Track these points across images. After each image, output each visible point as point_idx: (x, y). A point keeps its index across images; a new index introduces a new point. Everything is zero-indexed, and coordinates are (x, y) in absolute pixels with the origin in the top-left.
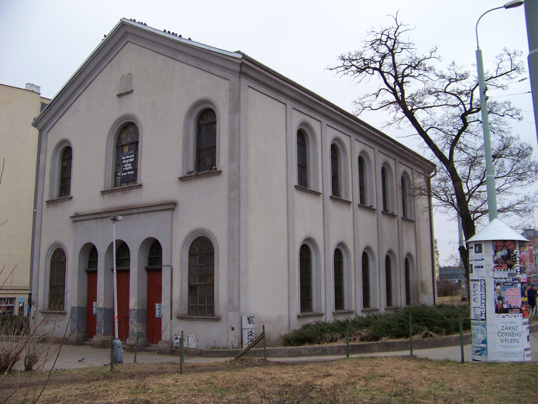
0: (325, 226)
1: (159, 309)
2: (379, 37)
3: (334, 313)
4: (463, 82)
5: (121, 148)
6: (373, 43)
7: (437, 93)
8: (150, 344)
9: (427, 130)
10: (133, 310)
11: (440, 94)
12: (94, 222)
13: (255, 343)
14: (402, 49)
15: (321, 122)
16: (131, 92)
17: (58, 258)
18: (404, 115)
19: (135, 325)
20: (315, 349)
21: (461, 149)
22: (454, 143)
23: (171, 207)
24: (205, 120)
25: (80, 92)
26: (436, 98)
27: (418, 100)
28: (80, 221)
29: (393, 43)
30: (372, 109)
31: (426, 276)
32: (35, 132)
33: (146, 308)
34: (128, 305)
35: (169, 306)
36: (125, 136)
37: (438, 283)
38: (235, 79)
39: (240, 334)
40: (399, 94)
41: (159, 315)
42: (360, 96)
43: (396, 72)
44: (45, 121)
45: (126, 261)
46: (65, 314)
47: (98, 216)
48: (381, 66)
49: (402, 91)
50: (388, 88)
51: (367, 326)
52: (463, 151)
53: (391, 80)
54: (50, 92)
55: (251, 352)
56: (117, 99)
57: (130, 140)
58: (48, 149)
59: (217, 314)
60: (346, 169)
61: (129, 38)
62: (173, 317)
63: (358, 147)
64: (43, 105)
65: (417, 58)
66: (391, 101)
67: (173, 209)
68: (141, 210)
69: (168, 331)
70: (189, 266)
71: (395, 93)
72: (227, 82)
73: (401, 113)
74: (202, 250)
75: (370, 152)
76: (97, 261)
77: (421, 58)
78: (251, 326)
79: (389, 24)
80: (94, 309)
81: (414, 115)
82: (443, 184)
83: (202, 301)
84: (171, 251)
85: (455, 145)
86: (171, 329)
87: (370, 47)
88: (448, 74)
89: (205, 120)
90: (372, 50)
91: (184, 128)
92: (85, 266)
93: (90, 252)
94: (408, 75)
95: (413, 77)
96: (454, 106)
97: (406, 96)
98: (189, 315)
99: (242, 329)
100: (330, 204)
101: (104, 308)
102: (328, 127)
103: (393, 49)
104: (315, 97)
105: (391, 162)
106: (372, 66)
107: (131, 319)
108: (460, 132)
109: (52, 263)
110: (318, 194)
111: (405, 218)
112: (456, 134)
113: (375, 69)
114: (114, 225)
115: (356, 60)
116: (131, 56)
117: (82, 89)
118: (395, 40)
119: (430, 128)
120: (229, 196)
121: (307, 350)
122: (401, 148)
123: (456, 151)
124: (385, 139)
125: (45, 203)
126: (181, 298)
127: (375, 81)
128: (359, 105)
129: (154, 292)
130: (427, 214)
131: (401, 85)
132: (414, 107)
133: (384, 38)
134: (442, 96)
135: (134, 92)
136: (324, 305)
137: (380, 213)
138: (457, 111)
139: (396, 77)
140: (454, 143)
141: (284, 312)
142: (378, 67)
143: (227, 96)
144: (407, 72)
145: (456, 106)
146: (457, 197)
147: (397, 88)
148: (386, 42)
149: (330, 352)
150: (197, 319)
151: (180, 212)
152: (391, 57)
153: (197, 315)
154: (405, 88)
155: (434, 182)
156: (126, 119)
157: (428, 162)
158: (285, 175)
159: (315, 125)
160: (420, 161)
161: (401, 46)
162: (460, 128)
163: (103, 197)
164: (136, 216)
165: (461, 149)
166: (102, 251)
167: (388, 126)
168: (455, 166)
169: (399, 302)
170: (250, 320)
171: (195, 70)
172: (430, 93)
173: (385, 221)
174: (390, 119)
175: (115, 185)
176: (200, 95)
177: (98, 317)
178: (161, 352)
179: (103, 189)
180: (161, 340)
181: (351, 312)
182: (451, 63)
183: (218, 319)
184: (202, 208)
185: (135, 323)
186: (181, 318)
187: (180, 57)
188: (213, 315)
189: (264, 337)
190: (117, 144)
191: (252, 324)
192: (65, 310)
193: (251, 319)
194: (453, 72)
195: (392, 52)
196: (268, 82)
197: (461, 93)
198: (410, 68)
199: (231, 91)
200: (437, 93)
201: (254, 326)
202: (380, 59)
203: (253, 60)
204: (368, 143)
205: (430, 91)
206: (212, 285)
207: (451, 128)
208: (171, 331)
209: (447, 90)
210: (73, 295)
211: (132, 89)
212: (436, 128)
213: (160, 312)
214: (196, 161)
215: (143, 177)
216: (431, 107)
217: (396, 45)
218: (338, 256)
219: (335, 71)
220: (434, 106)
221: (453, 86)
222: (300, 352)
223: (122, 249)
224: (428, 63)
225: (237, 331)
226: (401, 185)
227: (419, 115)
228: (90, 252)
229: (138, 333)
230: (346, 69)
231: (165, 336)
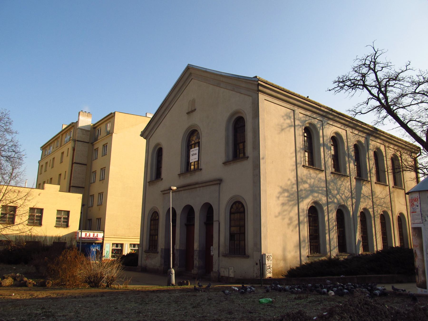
9: (407, 123)
14: (382, 68)
23: (218, 182)
25: (166, 113)
42: (353, 103)
46: (158, 253)
49: (386, 98)
53: (375, 91)
62: (220, 256)
67: (220, 184)
68: (201, 185)
71: (378, 99)
88: (416, 79)
91: (327, 107)
116: (194, 88)
125: (148, 183)
147: (381, 96)
154: (388, 94)
164: (198, 189)
166: (179, 212)
180: (212, 271)
183: (248, 257)
185: (197, 259)
186: (225, 256)
194: (421, 78)
208: (219, 265)
212: (415, 121)
227: (400, 113)
231: (215, 268)
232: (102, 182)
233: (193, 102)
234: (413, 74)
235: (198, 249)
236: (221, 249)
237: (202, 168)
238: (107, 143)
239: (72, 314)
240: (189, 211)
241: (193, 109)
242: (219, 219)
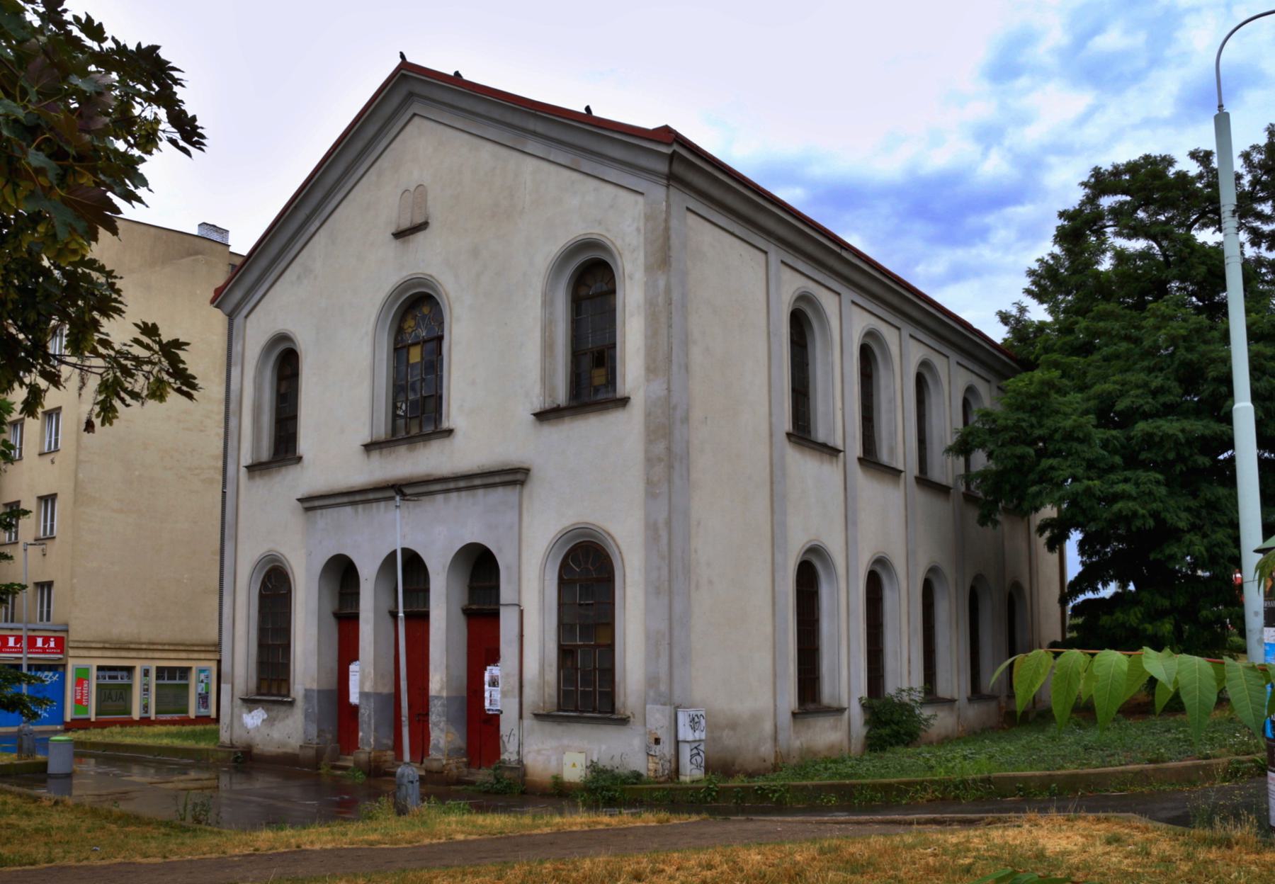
0: (849, 520)
5: (405, 351)
10: (437, 697)
12: (349, 509)
15: (839, 294)
17: (275, 585)
19: (442, 730)
23: (519, 477)
24: (589, 279)
25: (313, 229)
28: (321, 507)
33: (465, 694)
38: (658, 192)
39: (673, 752)
44: (238, 295)
45: (421, 594)
47: (358, 498)
56: (395, 244)
57: (423, 333)
60: (892, 400)
61: (416, 107)
62: (526, 713)
63: (917, 353)
67: (522, 483)
68: (452, 485)
72: (640, 199)
74: (586, 570)
75: (938, 361)
76: (358, 594)
89: (589, 279)
91: (544, 303)
92: (331, 606)
93: (342, 573)
98: (559, 710)
99: (677, 742)
101: (376, 694)
102: (855, 309)
107: (433, 718)
109: (263, 598)
117: (317, 224)
120: (646, 451)
125: (243, 471)
135: (434, 224)
151: (536, 489)
158: (766, 409)
159: (828, 302)
163: (368, 456)
170: (694, 723)
171: (567, 173)
175: (394, 430)
176: (577, 230)
177: (362, 711)
179: (368, 440)
183: (624, 721)
184: (592, 478)
185: (442, 725)
187: (532, 146)
190: (396, 342)
192: (292, 694)
196: (730, 200)
199: (648, 218)
206: (611, 647)
210: (844, 675)
215: (455, 413)
223: (414, 564)
225: (666, 749)
228: (342, 573)
232: (48, 458)
235: (444, 694)
236: (527, 690)
239: (535, 748)
241: (419, 220)
242: (520, 599)
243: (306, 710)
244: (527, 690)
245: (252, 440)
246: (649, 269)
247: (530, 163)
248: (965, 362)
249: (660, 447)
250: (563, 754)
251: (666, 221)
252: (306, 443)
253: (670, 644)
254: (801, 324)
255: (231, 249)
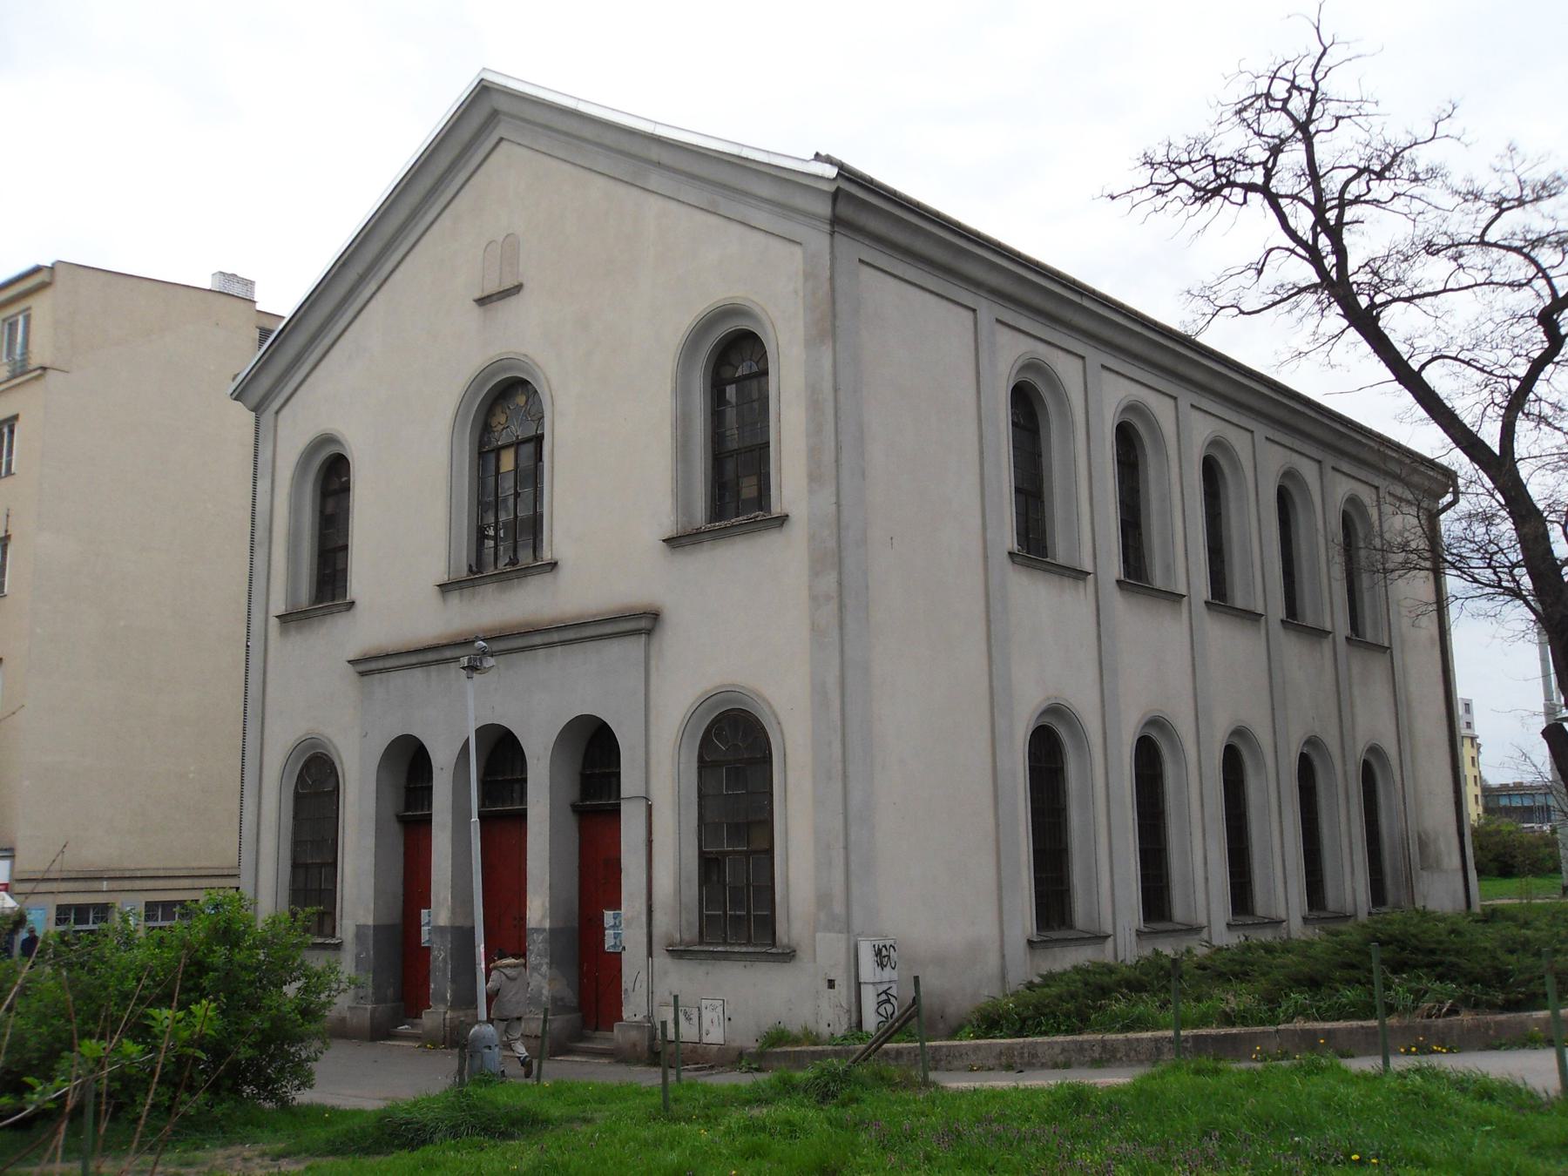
1: (614, 927)
2: (1262, 87)
3: (1139, 933)
4: (1546, 205)
6: (1245, 109)
7: (1455, 249)
8: (589, 1032)
9: (1423, 367)
10: (536, 930)
11: (1466, 249)
12: (418, 673)
13: (891, 1030)
14: (1338, 119)
16: (518, 288)
17: (315, 779)
18: (1345, 323)
19: (544, 976)
20: (1081, 1048)
21: (1541, 419)
22: (1516, 403)
23: (643, 624)
24: (731, 361)
25: (367, 293)
26: (1454, 265)
27: (1391, 276)
28: (380, 671)
29: (1307, 101)
30: (1242, 312)
31: (1436, 816)
32: (242, 416)
34: (523, 918)
35: (644, 918)
36: (503, 420)
37: (1475, 832)
40: (1330, 261)
41: (615, 946)
42: (1208, 277)
43: (1319, 193)
44: (265, 382)
45: (517, 787)
46: (338, 947)
47: (431, 656)
48: (1268, 176)
49: (1340, 252)
50: (1292, 245)
51: (1243, 976)
52: (1549, 424)
53: (1303, 220)
54: (281, 297)
55: (886, 1053)
56: (476, 310)
58: (279, 463)
59: (785, 941)
62: (658, 949)
64: (264, 333)
65: (1388, 145)
66: (1303, 284)
67: (649, 632)
68: (555, 637)
69: (642, 990)
70: (701, 796)
71: (1315, 258)
73: (1335, 319)
76: (431, 788)
77: (1404, 143)
78: (888, 974)
79: (1299, 46)
80: (425, 929)
81: (1380, 324)
82: (1480, 530)
83: (737, 903)
84: (647, 753)
85: (1520, 407)
86: (653, 987)
87: (1236, 119)
88: (1491, 185)
90: (1242, 129)
94: (1357, 200)
95: (1376, 202)
96: (1516, 285)
97: (1352, 265)
98: (701, 943)
100: (1117, 602)
102: (1105, 374)
103: (1309, 121)
104: (1065, 286)
105: (1308, 470)
106: (1243, 177)
108: (1537, 367)
109: (298, 798)
110: (1079, 575)
111: (1356, 637)
112: (1522, 370)
113: (1249, 187)
114: (469, 683)
115: (1190, 162)
116: (511, 177)
117: (373, 286)
118: (1314, 94)
119: (1434, 359)
120: (810, 588)
121: (1057, 1050)
122: (1338, 427)
123: (1523, 426)
124: (1285, 401)
125: (274, 622)
126: (679, 891)
127: (1252, 226)
128: (1201, 301)
129: (596, 877)
130: (1429, 625)
131: (1335, 234)
132: (1379, 299)
133: (1280, 90)
134: (1474, 256)
136: (1109, 910)
137: (1275, 625)
138: (1532, 300)
139: (1319, 209)
140: (1516, 403)
141: (986, 929)
142: (1259, 180)
143: (796, 292)
144: (1355, 189)
145: (1521, 285)
146: (1529, 573)
147: (1324, 242)
148: (1286, 101)
149: (1127, 1055)
150: (726, 956)
151: (671, 639)
152: (1301, 146)
153: (725, 943)
154: (1348, 238)
155: (1450, 525)
156: (505, 370)
157: (1431, 464)
158: (979, 521)
159: (1067, 370)
160: (1400, 462)
161: (1334, 108)
162: (1536, 354)
163: (444, 599)
164: (541, 652)
165: (1541, 419)
167: (1296, 361)
168: (1523, 474)
169: (1349, 898)
170: (882, 958)
172: (1431, 249)
173: (1292, 649)
174: (1301, 341)
176: (718, 294)
178: (620, 1056)
179: (444, 579)
180: (621, 1019)
181: (1192, 930)
182: (1502, 149)
183: (789, 956)
184: (741, 626)
185: (545, 969)
186: (678, 952)
187: (655, 180)
188: (774, 944)
189: (917, 1013)
190: (481, 444)
191: (888, 968)
193: (884, 952)
194: (1511, 180)
195: (1304, 128)
196: (919, 245)
197: (1540, 241)
198: (1365, 176)
199: (808, 276)
200: (1455, 249)
201: (894, 975)
202: (1265, 155)
203: (871, 181)
204: (1234, 417)
205: (1430, 244)
207: (1504, 355)
208: (650, 993)
209: (1489, 238)
211: (520, 280)
212: (1456, 359)
213: (617, 936)
214: (713, 487)
215: (559, 539)
216: (1435, 294)
217: (1319, 106)
218: (1148, 758)
219: (1124, 203)
220: (1445, 290)
221: (1512, 224)
222: (1035, 1056)
224: (1423, 158)
225: (843, 991)
226: (1340, 538)
227: (1397, 322)
228: (409, 763)
229: (554, 1000)
230: (1159, 192)
231: (633, 1008)
233: (510, 248)
234: (1473, 159)
235: (547, 925)
236: (662, 922)
237: (557, 557)
238: (16, 417)
240: (500, 753)
241: (507, 285)
242: (647, 791)
243: (357, 956)
244: (657, 915)
245: (285, 578)
246: (811, 343)
247: (654, 204)
248: (1278, 436)
249: (829, 582)
250: (723, 1003)
251: (832, 278)
252: (360, 579)
253: (846, 848)
254: (1027, 406)
255: (259, 307)
